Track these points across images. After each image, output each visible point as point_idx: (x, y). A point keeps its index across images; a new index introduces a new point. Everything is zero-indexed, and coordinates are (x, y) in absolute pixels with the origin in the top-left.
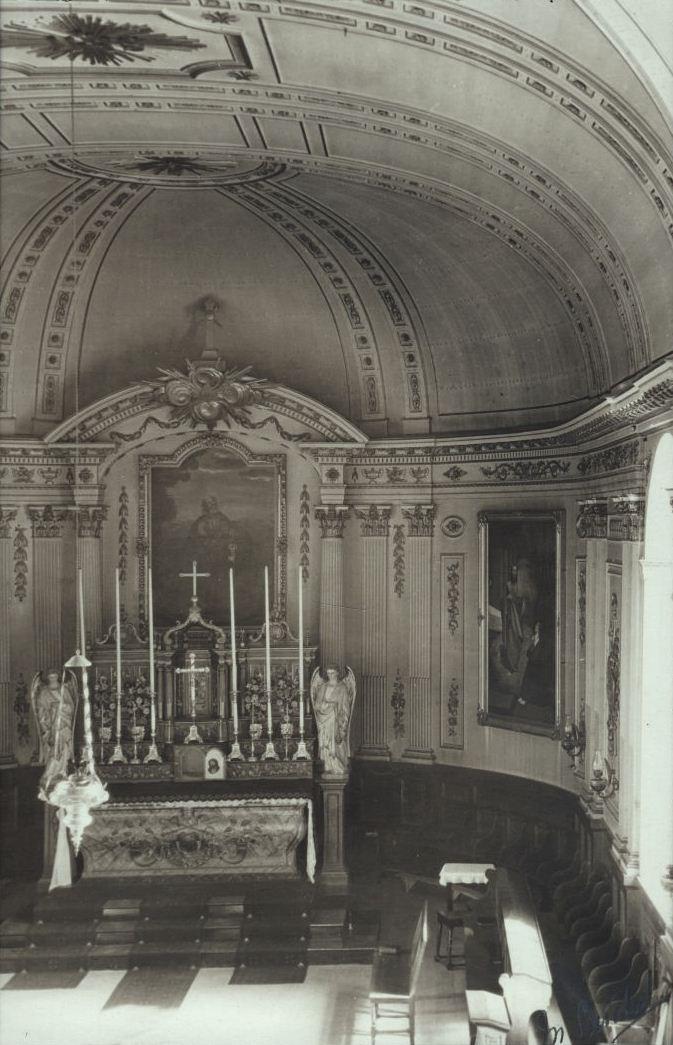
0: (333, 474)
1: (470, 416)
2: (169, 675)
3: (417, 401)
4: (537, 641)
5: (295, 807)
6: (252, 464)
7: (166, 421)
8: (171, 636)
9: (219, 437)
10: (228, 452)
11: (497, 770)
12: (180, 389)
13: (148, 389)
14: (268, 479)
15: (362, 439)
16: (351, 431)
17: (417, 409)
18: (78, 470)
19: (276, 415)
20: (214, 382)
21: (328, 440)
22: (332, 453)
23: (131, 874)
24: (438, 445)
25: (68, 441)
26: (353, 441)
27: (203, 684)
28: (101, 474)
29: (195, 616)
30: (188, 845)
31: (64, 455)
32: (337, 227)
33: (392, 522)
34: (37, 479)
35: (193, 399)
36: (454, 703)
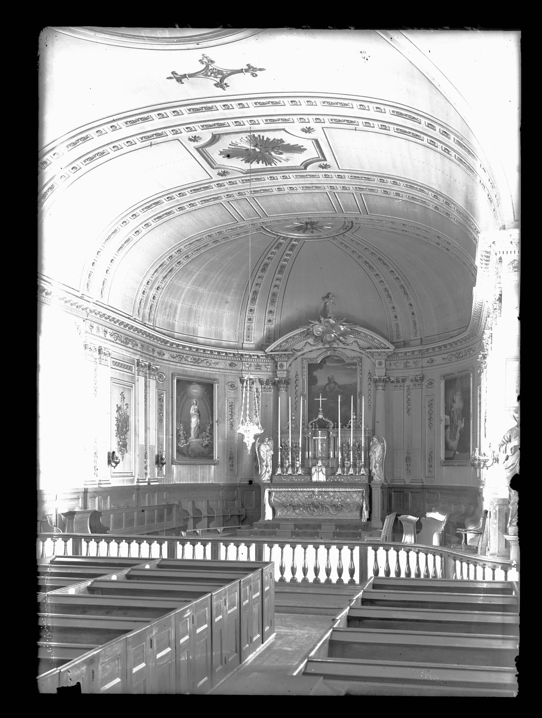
0: (380, 364)
1: (437, 336)
2: (310, 440)
3: (416, 332)
4: (463, 426)
5: (359, 491)
6: (347, 361)
7: (313, 344)
8: (312, 424)
9: (334, 349)
10: (338, 357)
11: (448, 485)
12: (318, 329)
13: (305, 329)
14: (354, 367)
15: (392, 347)
16: (388, 344)
17: (416, 336)
18: (279, 363)
19: (358, 340)
20: (333, 326)
21: (378, 348)
22: (380, 354)
23: (294, 517)
24: (424, 348)
25: (275, 351)
26: (388, 348)
27: (324, 445)
28: (287, 366)
29: (321, 416)
30: (316, 506)
31: (273, 358)
32: (379, 256)
33: (405, 384)
34: (263, 368)
35: (324, 333)
36: (431, 459)
